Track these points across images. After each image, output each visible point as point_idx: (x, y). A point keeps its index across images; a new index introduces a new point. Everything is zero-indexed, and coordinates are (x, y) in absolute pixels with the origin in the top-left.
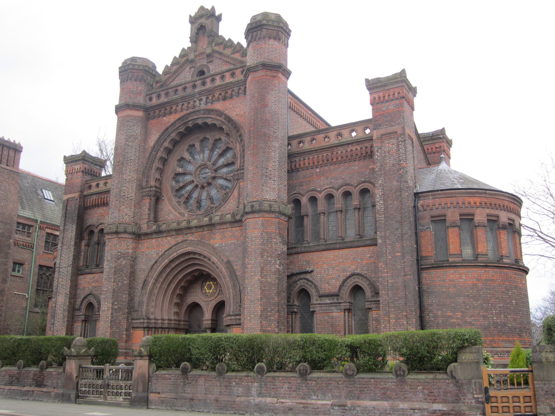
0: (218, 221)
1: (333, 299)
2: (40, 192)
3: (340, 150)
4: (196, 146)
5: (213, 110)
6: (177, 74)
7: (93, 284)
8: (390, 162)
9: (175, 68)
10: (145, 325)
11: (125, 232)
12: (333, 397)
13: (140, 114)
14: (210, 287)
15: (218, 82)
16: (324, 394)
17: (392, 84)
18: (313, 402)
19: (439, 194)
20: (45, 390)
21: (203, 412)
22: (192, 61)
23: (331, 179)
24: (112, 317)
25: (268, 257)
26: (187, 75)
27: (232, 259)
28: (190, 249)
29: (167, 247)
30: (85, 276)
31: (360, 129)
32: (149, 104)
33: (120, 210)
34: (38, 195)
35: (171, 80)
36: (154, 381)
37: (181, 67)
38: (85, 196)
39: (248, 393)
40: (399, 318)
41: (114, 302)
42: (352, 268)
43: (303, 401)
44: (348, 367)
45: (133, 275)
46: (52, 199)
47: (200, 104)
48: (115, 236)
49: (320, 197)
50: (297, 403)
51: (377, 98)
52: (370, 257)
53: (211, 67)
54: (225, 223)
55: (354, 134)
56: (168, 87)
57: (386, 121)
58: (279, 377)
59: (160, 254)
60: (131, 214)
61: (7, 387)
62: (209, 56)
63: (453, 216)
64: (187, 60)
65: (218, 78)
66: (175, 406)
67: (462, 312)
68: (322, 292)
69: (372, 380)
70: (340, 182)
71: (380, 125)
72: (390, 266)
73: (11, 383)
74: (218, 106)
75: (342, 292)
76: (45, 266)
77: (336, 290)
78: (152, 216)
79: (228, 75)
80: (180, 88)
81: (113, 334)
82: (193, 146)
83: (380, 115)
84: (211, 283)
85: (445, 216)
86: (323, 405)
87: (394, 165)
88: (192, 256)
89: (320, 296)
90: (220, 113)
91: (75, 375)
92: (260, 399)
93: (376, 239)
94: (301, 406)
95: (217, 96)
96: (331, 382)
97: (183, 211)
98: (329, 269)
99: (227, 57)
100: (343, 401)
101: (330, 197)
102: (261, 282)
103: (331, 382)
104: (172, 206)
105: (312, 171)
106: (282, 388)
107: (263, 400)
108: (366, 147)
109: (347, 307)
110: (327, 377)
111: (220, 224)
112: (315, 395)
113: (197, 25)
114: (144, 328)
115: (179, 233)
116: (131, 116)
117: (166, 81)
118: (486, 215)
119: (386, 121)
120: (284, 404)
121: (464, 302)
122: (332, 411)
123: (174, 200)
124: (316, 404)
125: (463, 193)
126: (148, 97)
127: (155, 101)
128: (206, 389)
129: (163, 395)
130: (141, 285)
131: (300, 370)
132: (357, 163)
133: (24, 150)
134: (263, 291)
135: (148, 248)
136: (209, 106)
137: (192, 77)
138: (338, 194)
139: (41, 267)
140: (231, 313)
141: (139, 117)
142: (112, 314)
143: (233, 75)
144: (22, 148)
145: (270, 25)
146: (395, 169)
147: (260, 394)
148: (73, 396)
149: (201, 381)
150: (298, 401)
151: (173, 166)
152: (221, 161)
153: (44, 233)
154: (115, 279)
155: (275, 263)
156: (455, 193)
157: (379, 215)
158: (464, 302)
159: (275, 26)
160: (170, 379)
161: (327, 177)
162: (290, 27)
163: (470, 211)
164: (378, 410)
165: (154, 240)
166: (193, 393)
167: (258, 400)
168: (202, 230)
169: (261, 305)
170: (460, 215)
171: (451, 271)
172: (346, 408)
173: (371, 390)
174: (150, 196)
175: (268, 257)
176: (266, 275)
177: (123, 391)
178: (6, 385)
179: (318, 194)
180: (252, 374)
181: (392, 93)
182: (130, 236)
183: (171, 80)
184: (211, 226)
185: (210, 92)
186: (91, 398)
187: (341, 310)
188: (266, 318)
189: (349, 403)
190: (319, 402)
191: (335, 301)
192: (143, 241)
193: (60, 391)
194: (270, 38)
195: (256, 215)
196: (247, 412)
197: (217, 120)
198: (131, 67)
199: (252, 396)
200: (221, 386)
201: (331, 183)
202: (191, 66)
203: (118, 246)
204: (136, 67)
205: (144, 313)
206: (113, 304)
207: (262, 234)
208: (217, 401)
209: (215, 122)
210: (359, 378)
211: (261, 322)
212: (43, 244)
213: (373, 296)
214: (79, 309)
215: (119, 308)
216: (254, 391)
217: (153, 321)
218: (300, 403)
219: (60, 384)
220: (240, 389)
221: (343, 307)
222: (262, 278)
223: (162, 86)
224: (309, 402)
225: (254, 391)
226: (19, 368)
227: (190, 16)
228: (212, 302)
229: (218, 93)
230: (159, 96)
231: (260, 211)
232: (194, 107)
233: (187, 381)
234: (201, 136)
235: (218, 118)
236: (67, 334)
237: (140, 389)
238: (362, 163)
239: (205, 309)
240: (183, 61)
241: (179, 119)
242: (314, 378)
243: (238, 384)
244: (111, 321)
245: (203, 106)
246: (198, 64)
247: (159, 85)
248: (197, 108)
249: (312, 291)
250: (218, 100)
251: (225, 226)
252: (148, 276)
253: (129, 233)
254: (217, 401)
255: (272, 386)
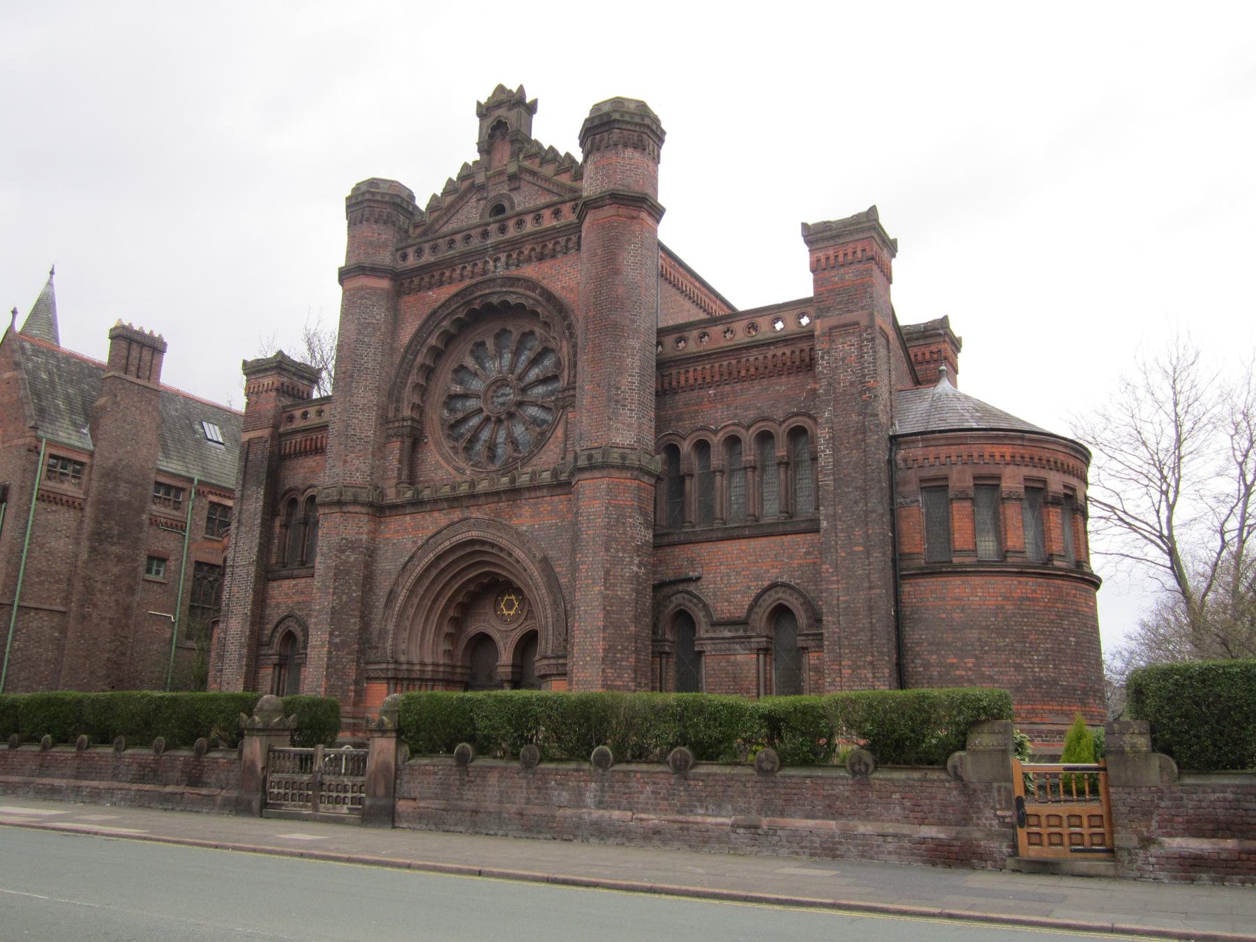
0: (527, 484)
1: (737, 630)
2: (197, 427)
3: (753, 356)
4: (488, 345)
5: (518, 279)
6: (453, 211)
7: (296, 598)
8: (845, 378)
9: (450, 199)
10: (390, 674)
11: (355, 502)
12: (736, 811)
13: (384, 284)
14: (510, 606)
15: (529, 227)
16: (719, 806)
17: (851, 233)
18: (699, 819)
19: (935, 439)
20: (204, 791)
21: (495, 835)
22: (482, 188)
23: (736, 408)
24: (329, 659)
25: (617, 550)
26: (472, 213)
27: (551, 553)
28: (474, 534)
29: (432, 530)
30: (280, 582)
31: (790, 316)
32: (401, 266)
33: (345, 462)
34: (195, 432)
35: (441, 222)
36: (406, 778)
37: (461, 198)
38: (281, 435)
39: (578, 802)
40: (859, 668)
41: (333, 630)
42: (773, 574)
43: (680, 818)
44: (763, 756)
45: (368, 582)
46: (221, 440)
47: (496, 267)
48: (336, 509)
49: (716, 440)
50: (669, 821)
51: (823, 260)
52: (805, 554)
53: (517, 198)
54: (540, 488)
55: (779, 326)
56: (436, 235)
57: (840, 303)
58: (636, 772)
59: (420, 543)
60: (366, 468)
61: (135, 787)
62: (513, 178)
63: (961, 479)
64: (473, 185)
65: (529, 219)
66: (444, 823)
67: (976, 657)
68: (716, 616)
69: (808, 781)
70: (752, 414)
71: (828, 310)
72: (843, 570)
73: (141, 779)
74: (529, 271)
75: (753, 616)
76: (206, 564)
77: (741, 613)
78: (405, 472)
79: (547, 213)
80: (458, 237)
81: (330, 689)
82: (483, 344)
83: (831, 291)
84: (513, 597)
85: (946, 478)
86: (717, 824)
87: (852, 384)
88: (477, 548)
89: (715, 624)
90: (532, 285)
91: (260, 765)
92: (601, 812)
93: (816, 521)
94: (676, 826)
95: (526, 252)
96: (731, 783)
97: (462, 464)
98: (732, 574)
99: (547, 180)
100: (753, 818)
101: (733, 442)
102: (605, 597)
103: (731, 783)
104: (442, 455)
105: (702, 393)
106: (642, 793)
107: (606, 814)
108: (802, 351)
109: (763, 645)
110: (725, 775)
111: (530, 489)
112: (701, 806)
113: (490, 121)
114: (388, 679)
115: (455, 504)
116: (367, 288)
117: (432, 225)
118: (1021, 478)
119: (840, 303)
120: (644, 823)
121: (979, 639)
122: (733, 836)
123: (447, 445)
124: (703, 823)
125: (979, 437)
126: (399, 253)
127: (412, 261)
128: (501, 792)
129: (422, 804)
130: (383, 601)
131: (674, 760)
132: (784, 379)
133: (168, 349)
134: (607, 614)
135: (398, 532)
136: (514, 272)
137: (482, 217)
138: (748, 437)
139: (199, 564)
140: (549, 653)
141: (382, 289)
142: (330, 652)
143: (557, 213)
144: (165, 345)
145: (627, 123)
146: (854, 390)
147: (600, 804)
148: (256, 804)
149: (493, 779)
150: (671, 818)
151: (445, 382)
152: (534, 373)
153: (204, 503)
154: (335, 588)
155: (631, 563)
156: (966, 437)
157: (826, 475)
158: (979, 639)
159: (636, 124)
160: (435, 773)
161: (729, 406)
162: (663, 126)
163: (994, 470)
164: (818, 836)
165: (408, 518)
166: (477, 801)
167: (597, 814)
168: (496, 499)
169: (604, 639)
170: (975, 478)
171: (956, 581)
172: (760, 831)
173: (806, 799)
174: (402, 436)
175: (617, 550)
176: (615, 585)
177: (349, 795)
178: (132, 782)
179: (712, 436)
180: (586, 766)
181: (851, 251)
182: (364, 510)
183: (441, 222)
184: (514, 492)
185: (514, 244)
186: (290, 807)
187: (751, 650)
188: (613, 663)
189: (765, 822)
190: (710, 820)
191: (741, 633)
192: (388, 519)
193: (234, 794)
194: (625, 146)
195: (597, 474)
196: (576, 837)
197: (527, 296)
198: (368, 196)
199: (585, 807)
200: (528, 788)
201: (735, 415)
202: (479, 196)
203: (341, 528)
204: (378, 198)
205: (389, 652)
206: (331, 634)
207: (607, 508)
208: (521, 815)
209: (522, 301)
210: (785, 777)
211: (603, 670)
212: (203, 523)
213: (810, 626)
214: (269, 644)
215: (342, 642)
216: (589, 798)
217: (405, 667)
218: (674, 822)
219: (232, 782)
220: (565, 793)
221: (754, 646)
222: (607, 589)
223: (425, 233)
224: (691, 819)
225: (589, 798)
226: (157, 751)
227: (479, 103)
228: (514, 633)
229: (529, 247)
230: (419, 252)
231: (604, 466)
232: (485, 272)
233: (467, 779)
234: (496, 327)
235: (528, 293)
236: (245, 689)
237: (381, 791)
238: (793, 380)
239: (501, 645)
240: (465, 186)
241: (456, 295)
242: (701, 774)
243: (560, 784)
244: (328, 667)
245: (501, 272)
246: (493, 194)
247: (418, 231)
248: (490, 275)
249: (699, 616)
250: (529, 260)
251: (539, 494)
252: (396, 583)
253: (363, 505)
254: (521, 815)
255: (623, 790)
